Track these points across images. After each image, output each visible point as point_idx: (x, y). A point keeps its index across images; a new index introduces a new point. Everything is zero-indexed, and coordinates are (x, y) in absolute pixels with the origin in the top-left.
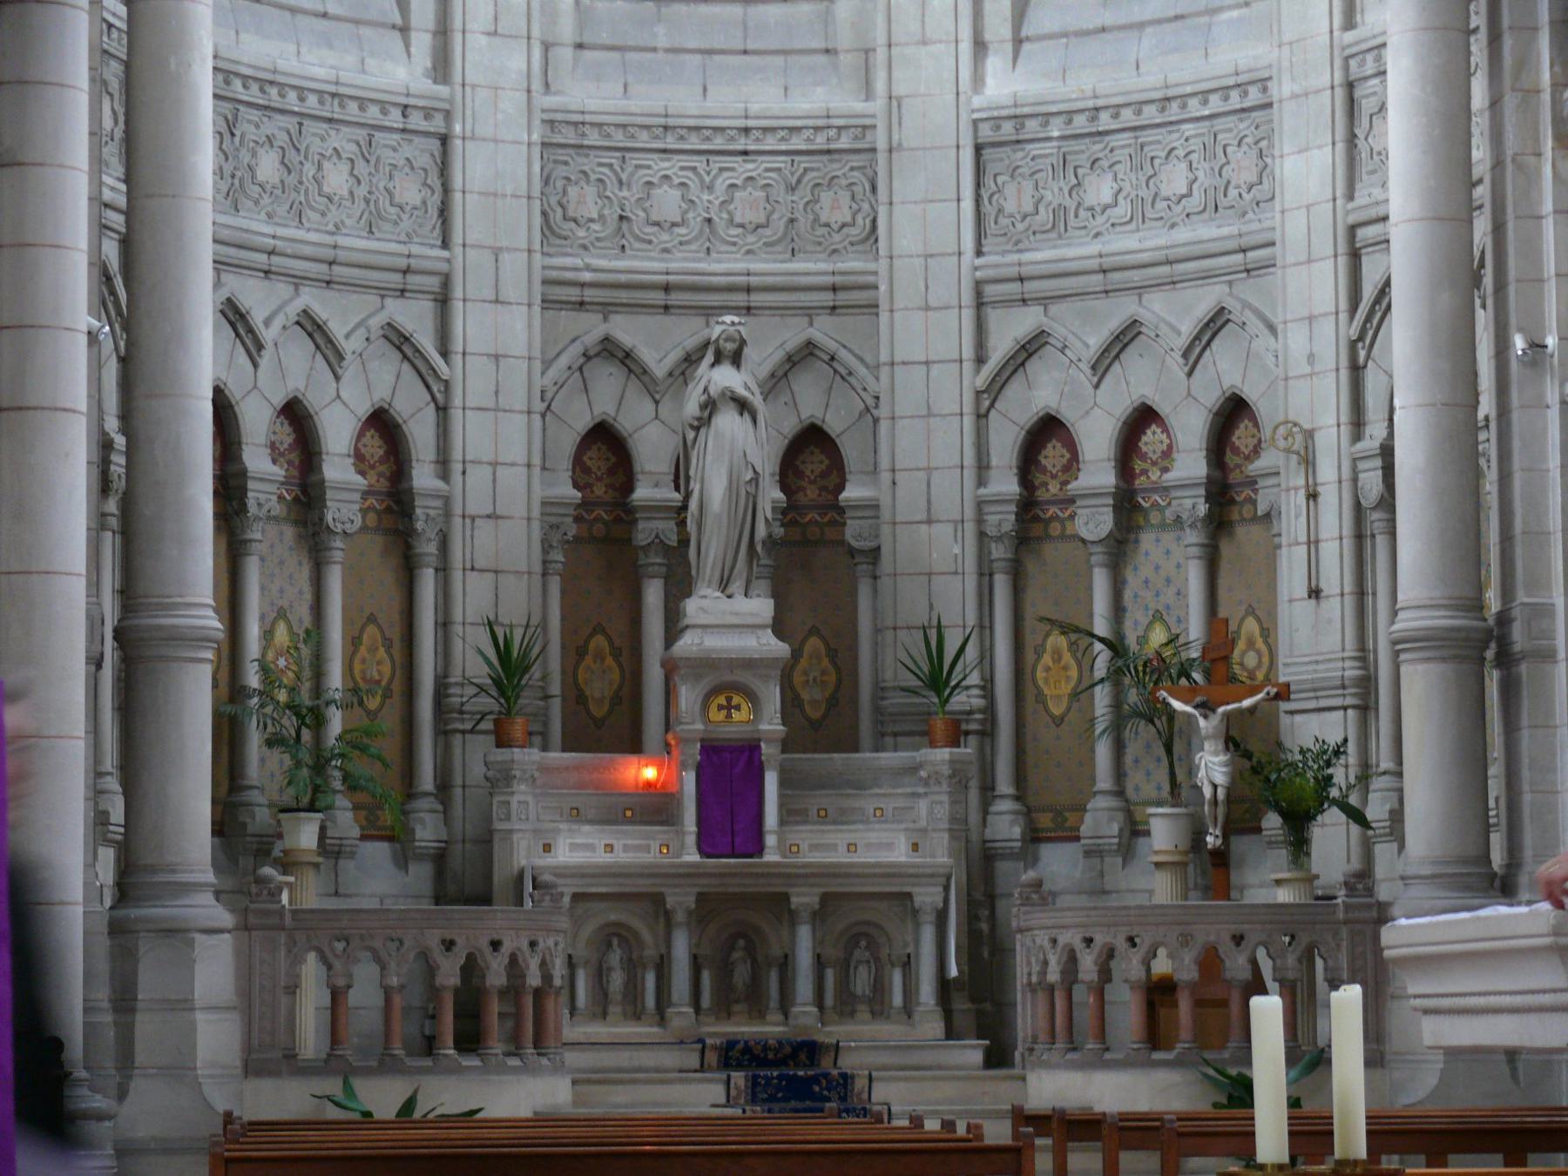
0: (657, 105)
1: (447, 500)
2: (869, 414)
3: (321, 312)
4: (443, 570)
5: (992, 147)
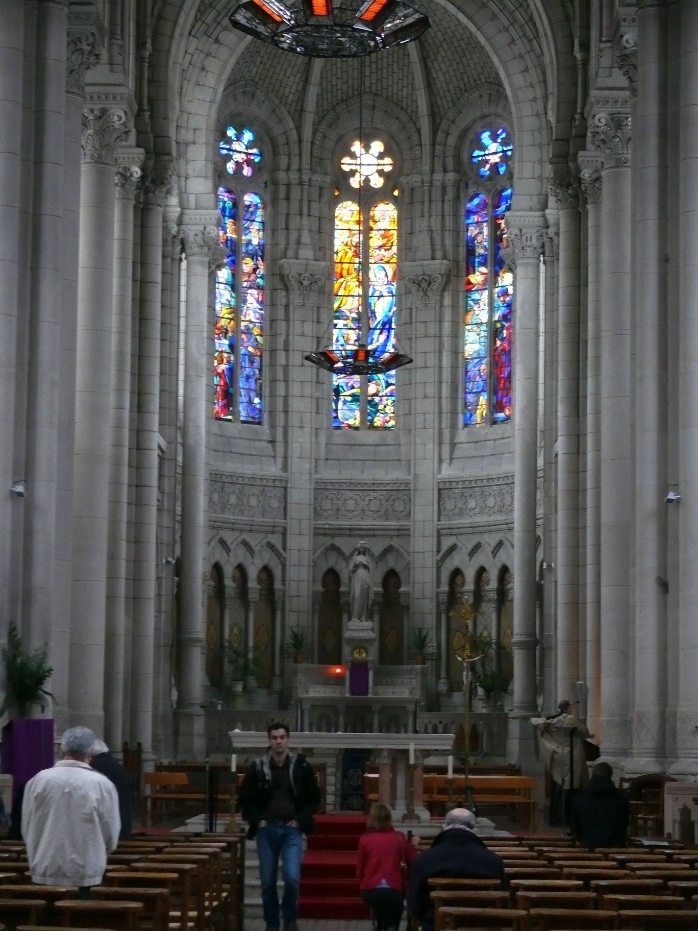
0: (348, 477)
1: (284, 591)
2: (408, 567)
3: (248, 540)
4: (283, 611)
5: (443, 490)
